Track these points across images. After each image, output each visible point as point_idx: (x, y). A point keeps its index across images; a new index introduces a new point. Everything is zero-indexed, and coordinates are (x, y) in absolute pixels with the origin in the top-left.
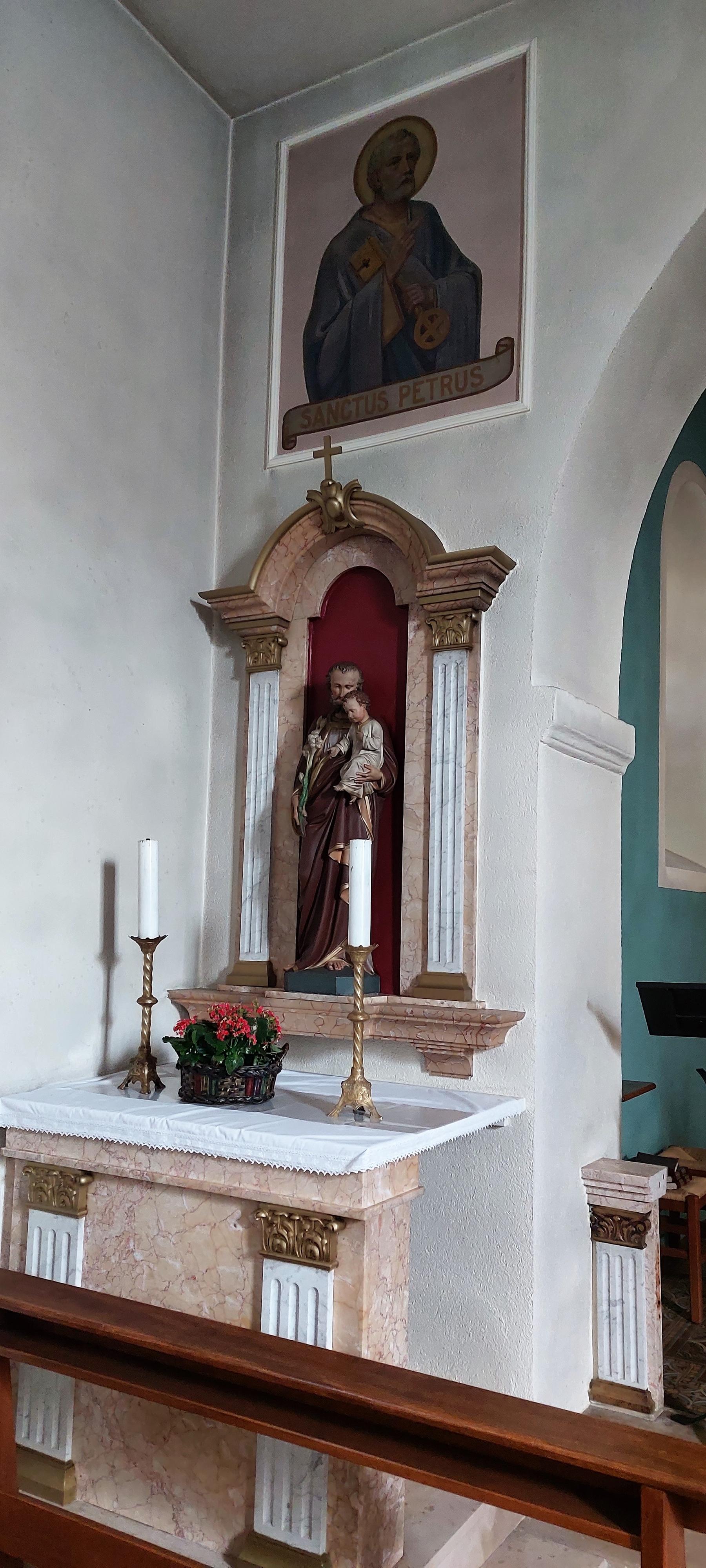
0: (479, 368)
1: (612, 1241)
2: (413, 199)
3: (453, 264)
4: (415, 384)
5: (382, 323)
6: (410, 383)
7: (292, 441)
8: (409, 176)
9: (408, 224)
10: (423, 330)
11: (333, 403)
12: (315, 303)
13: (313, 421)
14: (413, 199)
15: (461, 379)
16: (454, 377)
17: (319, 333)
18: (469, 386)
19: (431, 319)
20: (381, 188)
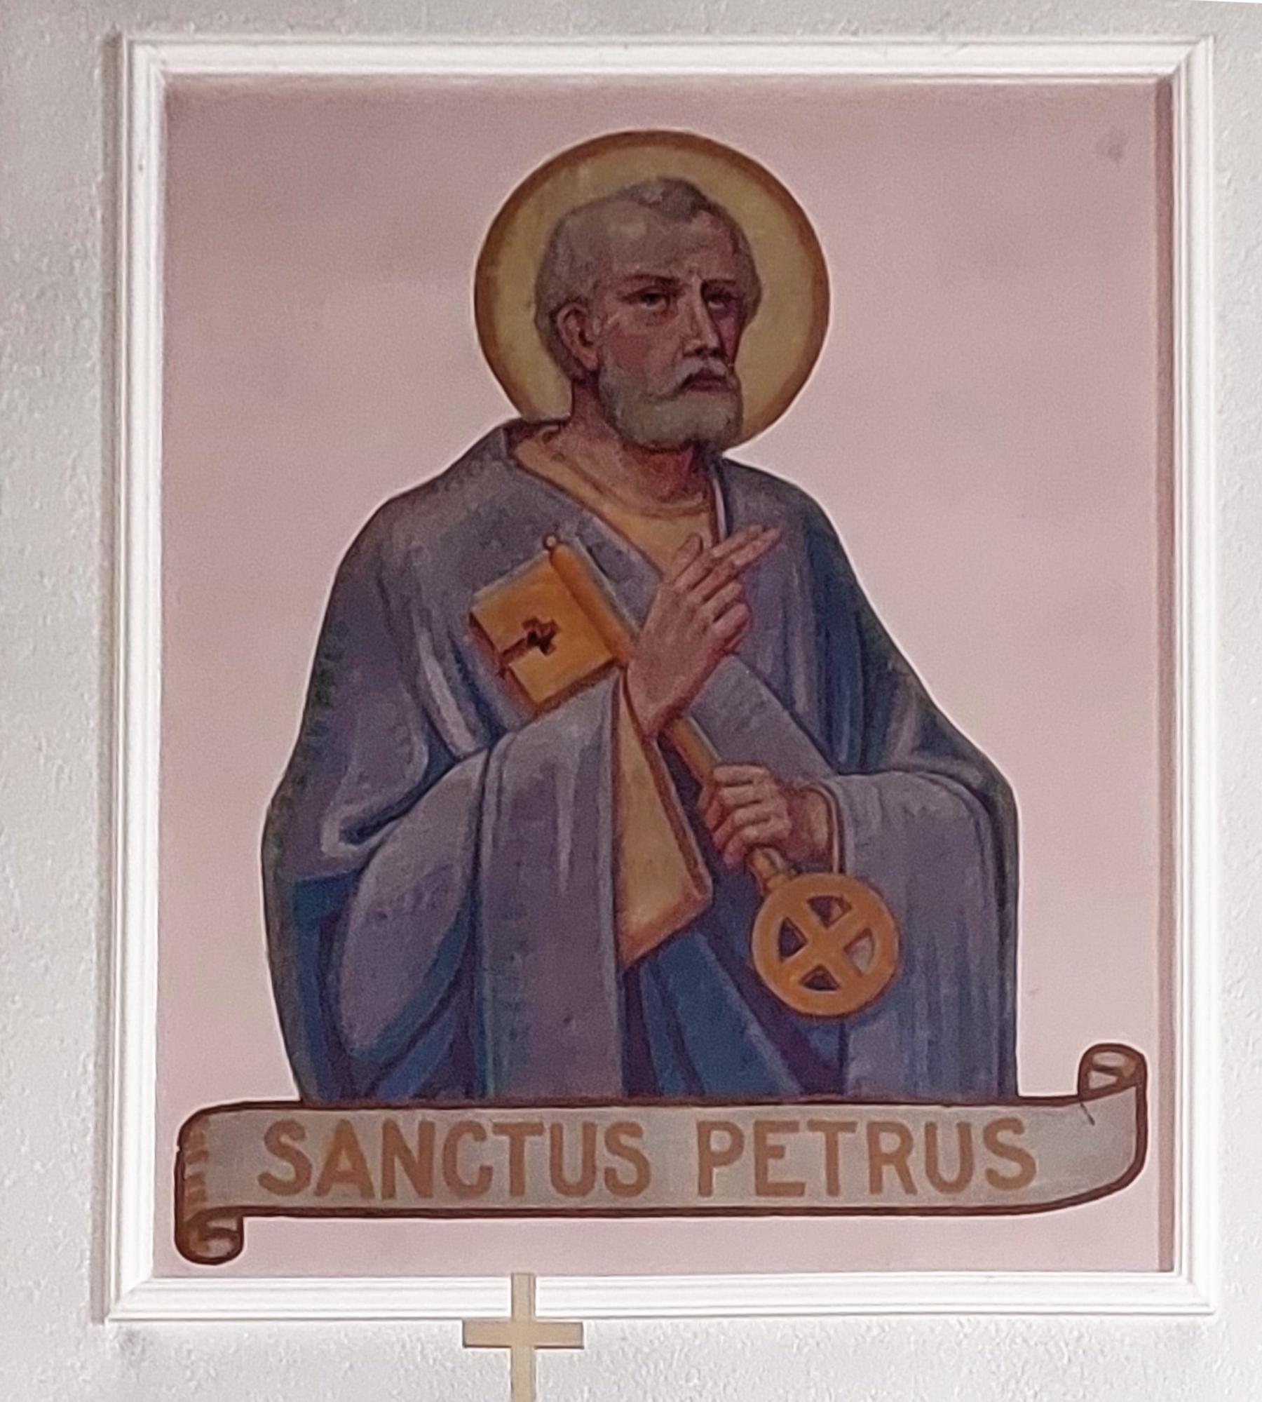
0: (1016, 1126)
1: (466, 1102)
2: (730, 454)
3: (905, 734)
4: (762, 1128)
5: (615, 872)
6: (744, 1116)
7: (220, 1233)
8: (718, 367)
9: (716, 542)
10: (789, 941)
11: (409, 1122)
12: (310, 728)
13: (316, 1174)
14: (730, 454)
15: (948, 1143)
16: (919, 1136)
17: (332, 843)
18: (978, 1177)
19: (822, 907)
20: (595, 374)
